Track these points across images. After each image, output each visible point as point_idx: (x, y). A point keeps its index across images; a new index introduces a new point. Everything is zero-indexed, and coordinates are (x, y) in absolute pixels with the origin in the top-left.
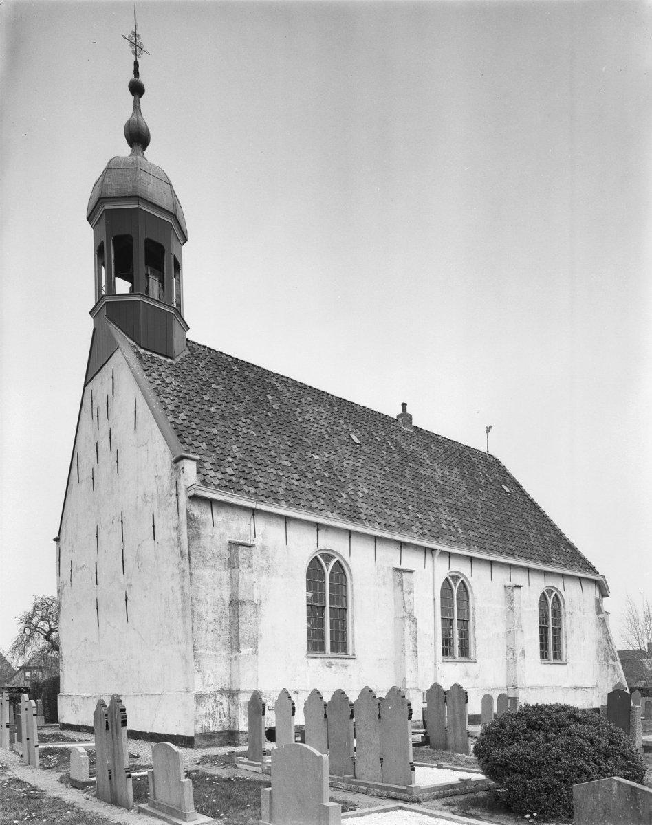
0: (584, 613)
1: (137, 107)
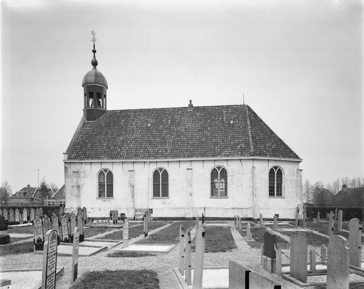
0: (242, 175)
1: (94, 56)
